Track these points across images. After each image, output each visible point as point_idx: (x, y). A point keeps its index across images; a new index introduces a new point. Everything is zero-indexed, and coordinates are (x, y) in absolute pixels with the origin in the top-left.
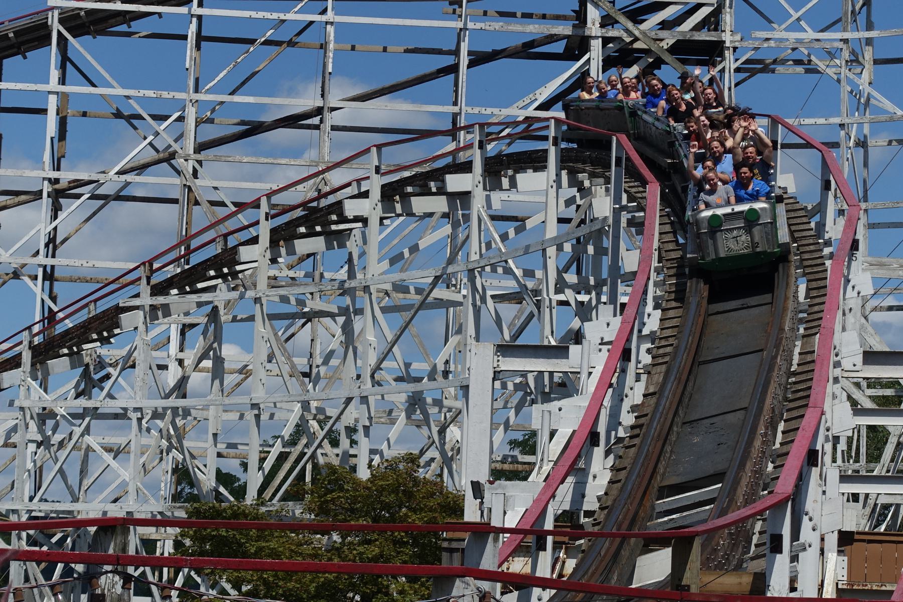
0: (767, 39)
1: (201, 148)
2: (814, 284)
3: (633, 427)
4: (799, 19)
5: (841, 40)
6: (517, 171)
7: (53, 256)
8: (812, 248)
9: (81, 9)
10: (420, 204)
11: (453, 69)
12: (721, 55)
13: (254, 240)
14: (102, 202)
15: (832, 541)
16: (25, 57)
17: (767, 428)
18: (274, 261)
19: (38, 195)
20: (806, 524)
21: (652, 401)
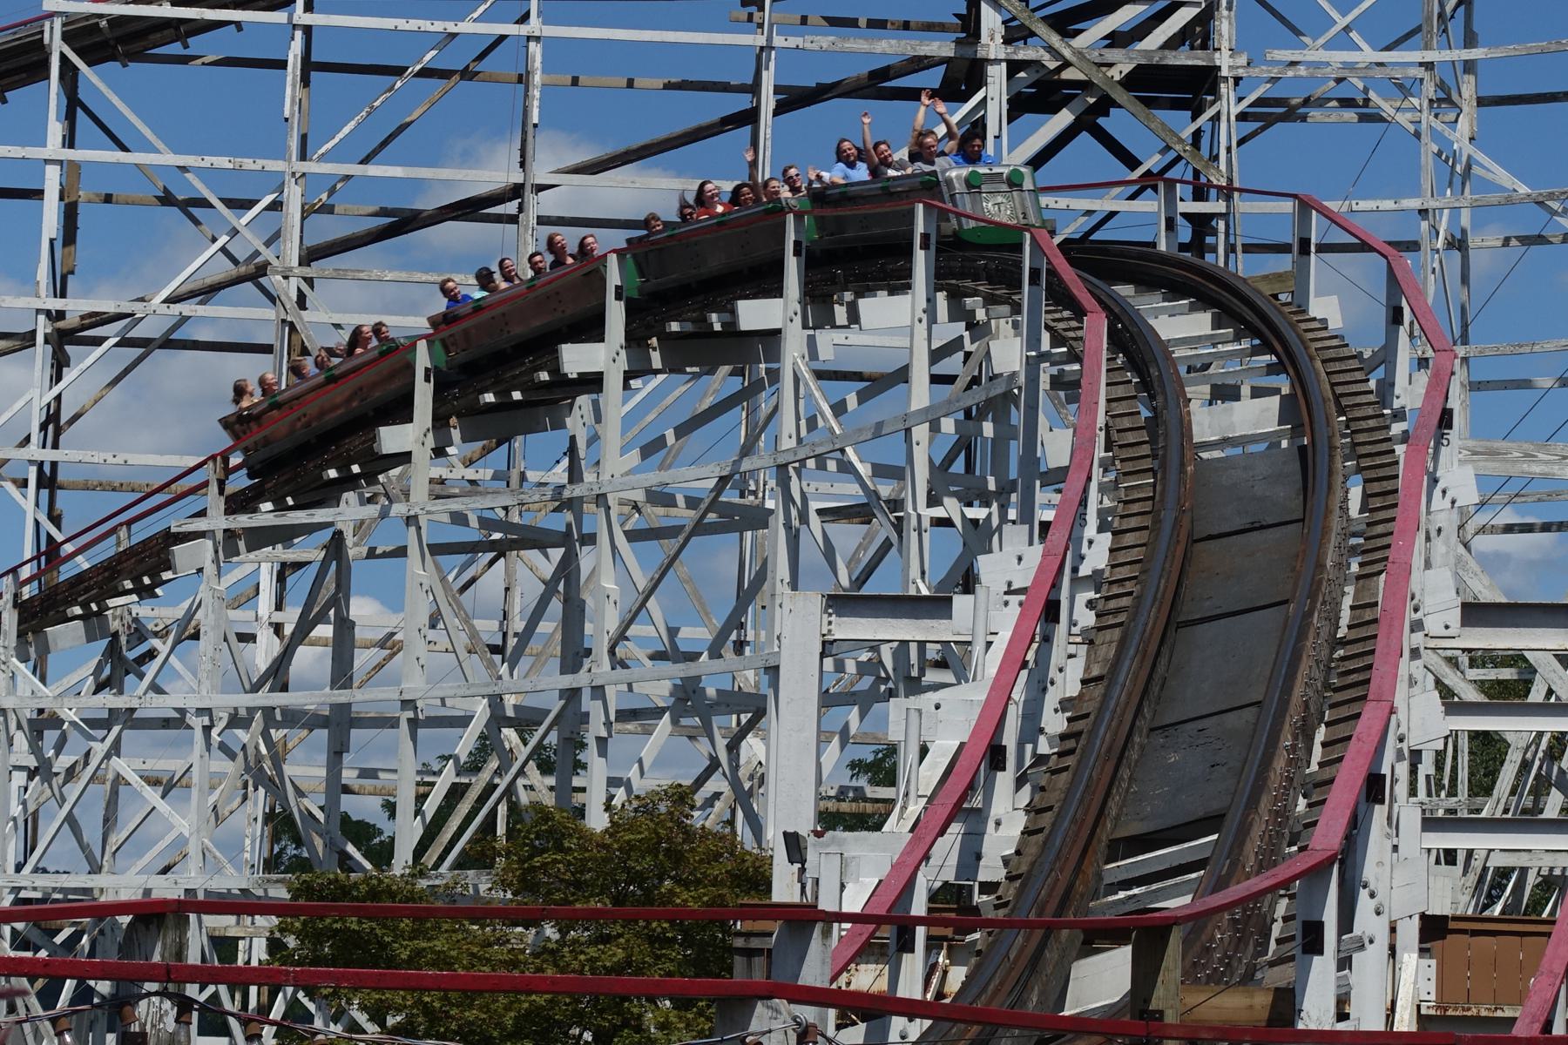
0: (1293, 64)
1: (311, 256)
2: (1376, 487)
3: (1063, 737)
4: (1347, 29)
5: (1421, 64)
6: (860, 294)
7: (55, 446)
8: (1372, 423)
9: (101, 16)
12: (1214, 91)
15: (1410, 932)
17: (1295, 738)
19: (28, 339)
20: (1364, 904)
21: (1098, 690)
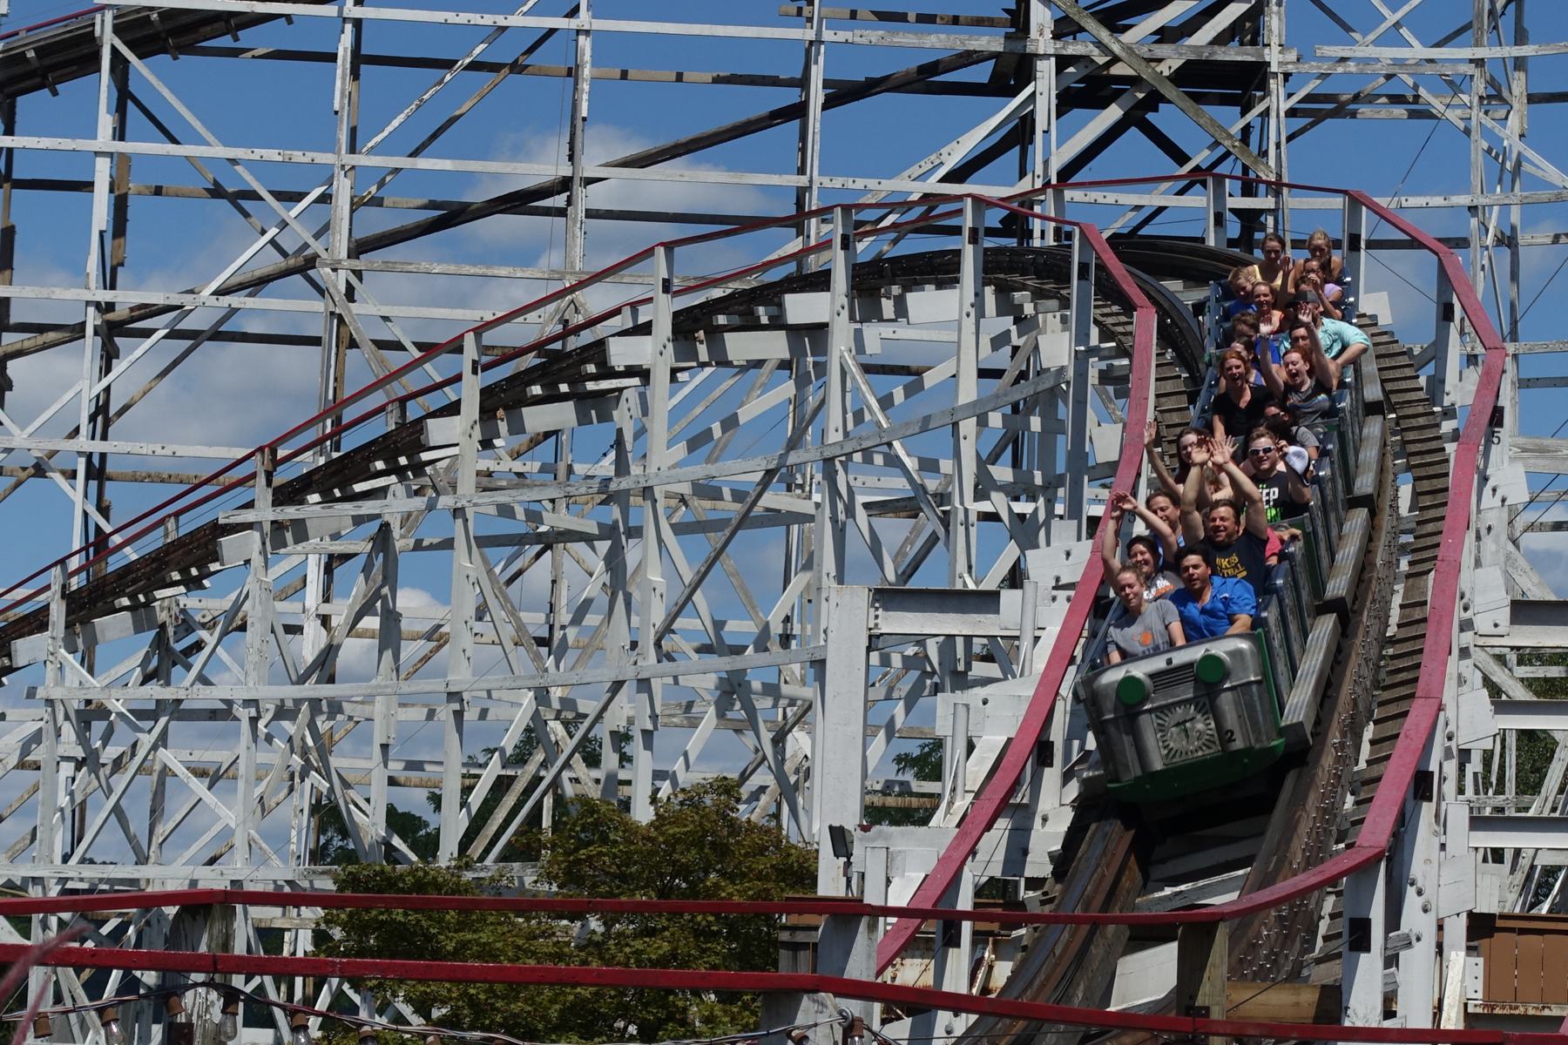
0: (1343, 60)
1: (359, 248)
2: (1426, 485)
4: (1397, 25)
5: (1471, 61)
6: (907, 288)
8: (1422, 421)
10: (740, 346)
11: (798, 111)
12: (1263, 86)
13: (453, 409)
14: (189, 343)
15: (1457, 930)
16: (55, 93)
17: (1344, 735)
18: (486, 444)
20: (1412, 902)
